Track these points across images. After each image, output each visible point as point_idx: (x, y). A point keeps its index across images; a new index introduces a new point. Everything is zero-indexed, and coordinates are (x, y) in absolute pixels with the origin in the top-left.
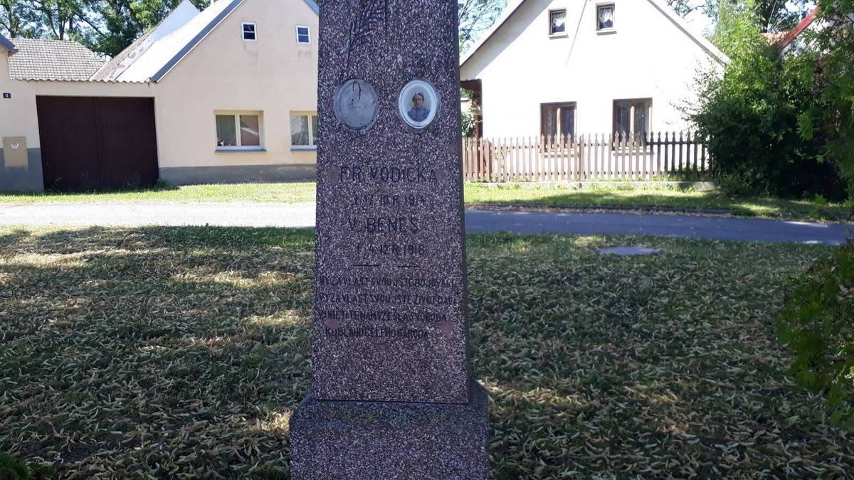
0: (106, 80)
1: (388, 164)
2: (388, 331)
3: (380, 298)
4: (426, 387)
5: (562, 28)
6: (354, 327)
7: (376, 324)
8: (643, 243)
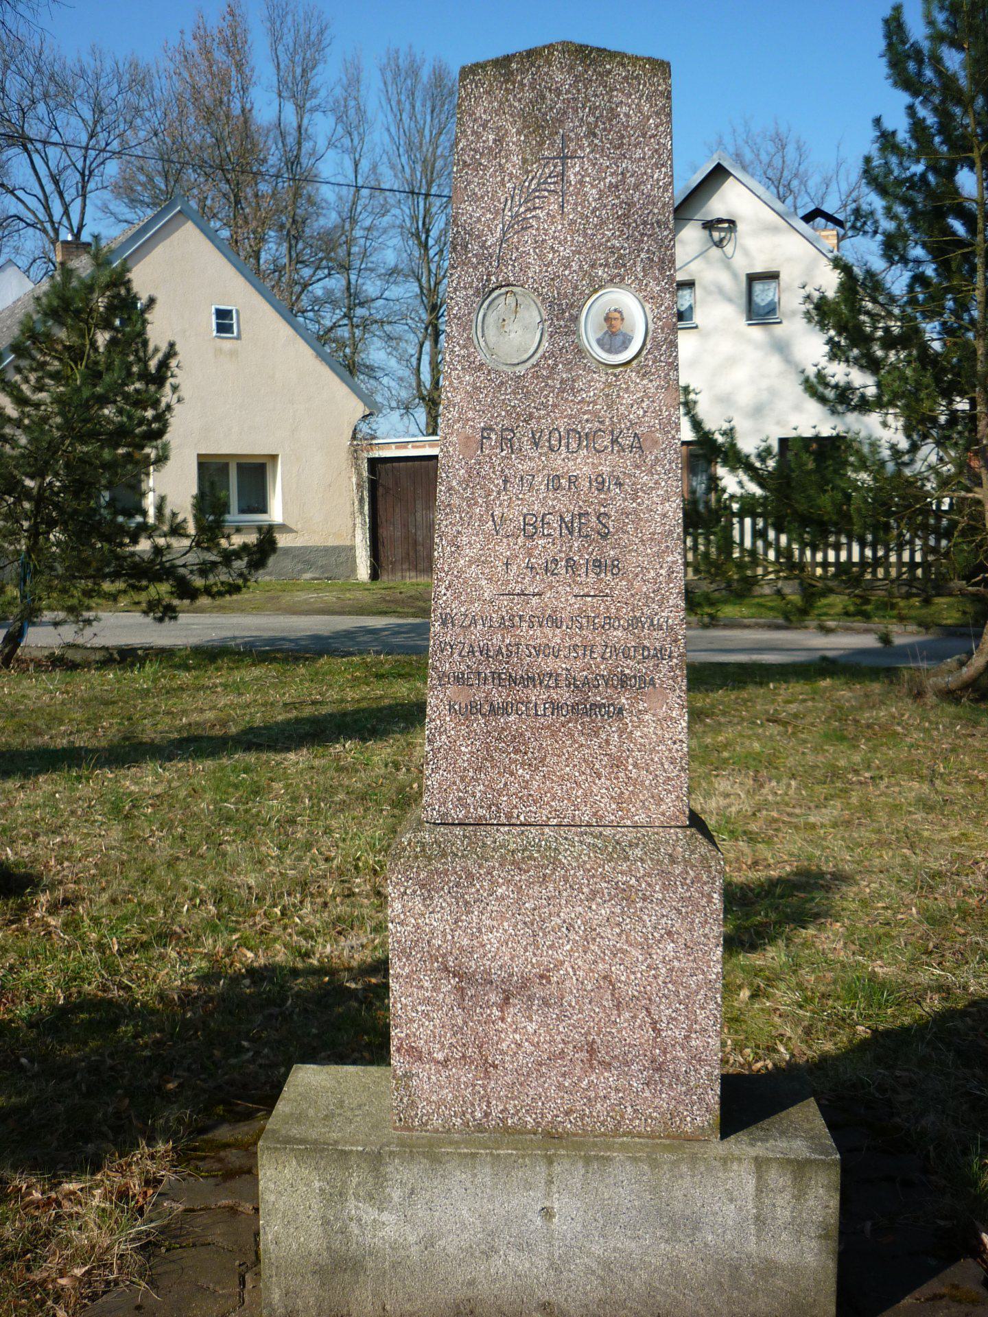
1: (562, 424)
2: (556, 707)
4: (619, 800)
6: (498, 700)
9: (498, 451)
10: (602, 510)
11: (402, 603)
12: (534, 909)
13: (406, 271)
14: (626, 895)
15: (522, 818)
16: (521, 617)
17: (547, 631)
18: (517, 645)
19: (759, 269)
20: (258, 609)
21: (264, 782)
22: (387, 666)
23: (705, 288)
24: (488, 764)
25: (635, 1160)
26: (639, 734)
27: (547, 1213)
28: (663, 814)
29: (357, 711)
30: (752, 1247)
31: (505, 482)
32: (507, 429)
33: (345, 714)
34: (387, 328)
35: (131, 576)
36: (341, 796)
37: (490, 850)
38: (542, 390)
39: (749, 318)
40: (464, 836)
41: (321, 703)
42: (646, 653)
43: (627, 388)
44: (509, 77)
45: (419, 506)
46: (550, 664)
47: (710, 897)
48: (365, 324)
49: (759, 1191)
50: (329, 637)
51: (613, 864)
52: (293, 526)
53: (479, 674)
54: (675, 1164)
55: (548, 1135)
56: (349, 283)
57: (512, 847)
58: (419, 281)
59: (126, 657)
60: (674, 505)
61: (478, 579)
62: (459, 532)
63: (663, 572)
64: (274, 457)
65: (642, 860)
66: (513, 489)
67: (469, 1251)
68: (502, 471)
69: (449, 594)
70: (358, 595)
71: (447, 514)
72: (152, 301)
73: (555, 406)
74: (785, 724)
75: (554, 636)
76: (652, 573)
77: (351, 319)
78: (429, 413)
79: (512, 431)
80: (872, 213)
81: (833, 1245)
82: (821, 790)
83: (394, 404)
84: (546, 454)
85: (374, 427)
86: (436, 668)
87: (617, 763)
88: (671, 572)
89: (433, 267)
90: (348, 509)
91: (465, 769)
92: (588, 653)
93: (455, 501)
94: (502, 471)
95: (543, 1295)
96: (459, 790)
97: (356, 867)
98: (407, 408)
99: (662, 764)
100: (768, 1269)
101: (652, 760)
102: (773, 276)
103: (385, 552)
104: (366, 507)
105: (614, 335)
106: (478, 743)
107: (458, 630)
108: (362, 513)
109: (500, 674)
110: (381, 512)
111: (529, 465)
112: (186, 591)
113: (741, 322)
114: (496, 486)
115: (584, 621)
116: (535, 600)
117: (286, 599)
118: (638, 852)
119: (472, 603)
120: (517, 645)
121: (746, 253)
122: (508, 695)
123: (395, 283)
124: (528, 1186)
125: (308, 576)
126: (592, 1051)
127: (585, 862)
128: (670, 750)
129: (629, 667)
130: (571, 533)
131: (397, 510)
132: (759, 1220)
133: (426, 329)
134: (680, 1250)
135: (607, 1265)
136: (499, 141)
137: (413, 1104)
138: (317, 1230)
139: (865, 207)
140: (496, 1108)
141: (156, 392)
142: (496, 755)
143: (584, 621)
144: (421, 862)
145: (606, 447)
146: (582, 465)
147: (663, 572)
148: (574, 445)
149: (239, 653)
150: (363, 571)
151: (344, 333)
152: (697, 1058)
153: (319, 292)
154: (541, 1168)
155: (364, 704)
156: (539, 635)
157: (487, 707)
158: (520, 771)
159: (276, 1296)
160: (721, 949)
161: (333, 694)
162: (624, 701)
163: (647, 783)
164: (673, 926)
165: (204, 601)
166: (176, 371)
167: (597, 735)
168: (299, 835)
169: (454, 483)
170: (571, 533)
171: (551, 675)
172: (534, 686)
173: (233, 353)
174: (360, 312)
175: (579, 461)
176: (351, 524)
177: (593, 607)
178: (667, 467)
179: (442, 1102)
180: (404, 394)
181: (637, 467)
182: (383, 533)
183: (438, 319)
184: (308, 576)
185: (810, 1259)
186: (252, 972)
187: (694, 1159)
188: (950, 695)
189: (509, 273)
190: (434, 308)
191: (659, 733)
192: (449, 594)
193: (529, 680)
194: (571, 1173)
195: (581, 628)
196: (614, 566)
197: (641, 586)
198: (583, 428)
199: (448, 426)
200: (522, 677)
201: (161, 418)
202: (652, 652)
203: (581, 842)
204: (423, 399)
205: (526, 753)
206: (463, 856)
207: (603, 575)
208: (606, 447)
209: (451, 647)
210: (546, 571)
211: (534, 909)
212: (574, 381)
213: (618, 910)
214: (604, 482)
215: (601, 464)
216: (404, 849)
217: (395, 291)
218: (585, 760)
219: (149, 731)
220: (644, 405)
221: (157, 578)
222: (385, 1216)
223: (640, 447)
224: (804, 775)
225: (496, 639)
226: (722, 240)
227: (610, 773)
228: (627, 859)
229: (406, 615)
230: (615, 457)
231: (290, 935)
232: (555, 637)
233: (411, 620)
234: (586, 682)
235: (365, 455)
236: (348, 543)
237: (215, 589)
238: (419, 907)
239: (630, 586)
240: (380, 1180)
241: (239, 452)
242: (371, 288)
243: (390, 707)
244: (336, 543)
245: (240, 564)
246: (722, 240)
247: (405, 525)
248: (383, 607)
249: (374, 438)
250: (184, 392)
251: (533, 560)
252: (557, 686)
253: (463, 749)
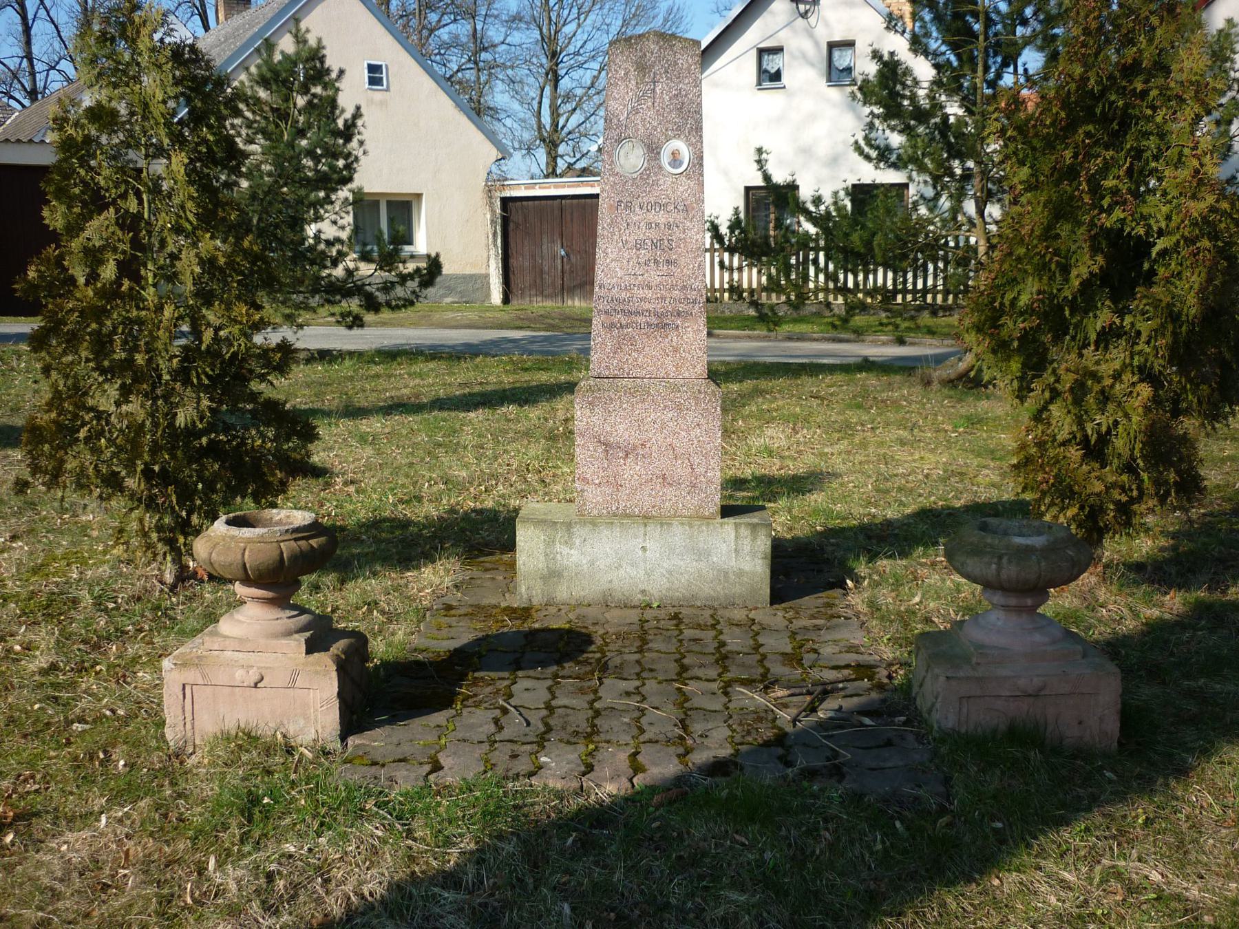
0: (36, 140)
1: (652, 200)
2: (649, 325)
3: (644, 300)
4: (677, 367)
5: (777, 76)
6: (624, 322)
7: (640, 319)
8: (1028, 846)
11: (534, 320)
13: (527, 18)
14: (679, 408)
19: (837, 38)
20: (415, 325)
21: (458, 426)
23: (791, 54)
25: (683, 524)
27: (644, 549)
30: (733, 563)
33: (504, 391)
34: (510, 72)
35: (327, 292)
36: (512, 435)
39: (829, 80)
44: (631, 46)
45: (545, 240)
46: (646, 306)
48: (492, 66)
49: (736, 537)
54: (700, 526)
55: (645, 517)
56: (475, 29)
58: (541, 30)
59: (324, 356)
64: (419, 196)
66: (631, 227)
67: (610, 567)
72: (342, 72)
74: (822, 399)
77: (476, 63)
78: (549, 153)
80: (901, 17)
81: (769, 562)
82: (836, 435)
83: (517, 145)
85: (504, 168)
87: (676, 350)
89: (554, 16)
90: (484, 241)
93: (606, 233)
95: (642, 587)
98: (529, 149)
100: (741, 573)
102: (850, 44)
104: (499, 240)
105: (675, 160)
108: (495, 245)
111: (637, 218)
112: (372, 305)
113: (822, 83)
117: (436, 317)
121: (827, 24)
123: (517, 29)
124: (636, 537)
125: (449, 300)
126: (664, 479)
129: (681, 307)
131: (526, 243)
132: (736, 551)
133: (547, 74)
134: (702, 565)
135: (670, 573)
136: (626, 74)
137: (584, 504)
138: (542, 558)
139: (896, 12)
140: (622, 504)
141: (344, 144)
144: (590, 393)
146: (661, 218)
149: (412, 353)
150: (496, 297)
151: (470, 75)
152: (710, 481)
153: (445, 37)
154: (642, 529)
155: (517, 385)
156: (642, 293)
159: (523, 589)
165: (386, 314)
166: (362, 129)
173: (383, 104)
174: (484, 56)
176: (485, 255)
179: (597, 503)
180: (527, 136)
183: (557, 65)
184: (449, 300)
185: (759, 569)
186: (474, 510)
187: (708, 524)
188: (951, 383)
189: (629, 132)
190: (554, 55)
193: (637, 313)
194: (654, 530)
201: (348, 167)
204: (544, 141)
217: (516, 37)
219: (361, 401)
221: (348, 294)
222: (573, 552)
224: (829, 427)
225: (623, 295)
226: (807, 12)
229: (539, 329)
232: (649, 294)
233: (542, 333)
235: (498, 194)
236: (483, 272)
237: (394, 303)
238: (588, 414)
240: (571, 535)
241: (389, 191)
242: (494, 33)
243: (537, 386)
244: (473, 272)
245: (413, 285)
246: (807, 12)
247: (533, 256)
248: (519, 323)
249: (506, 179)
250: (367, 146)
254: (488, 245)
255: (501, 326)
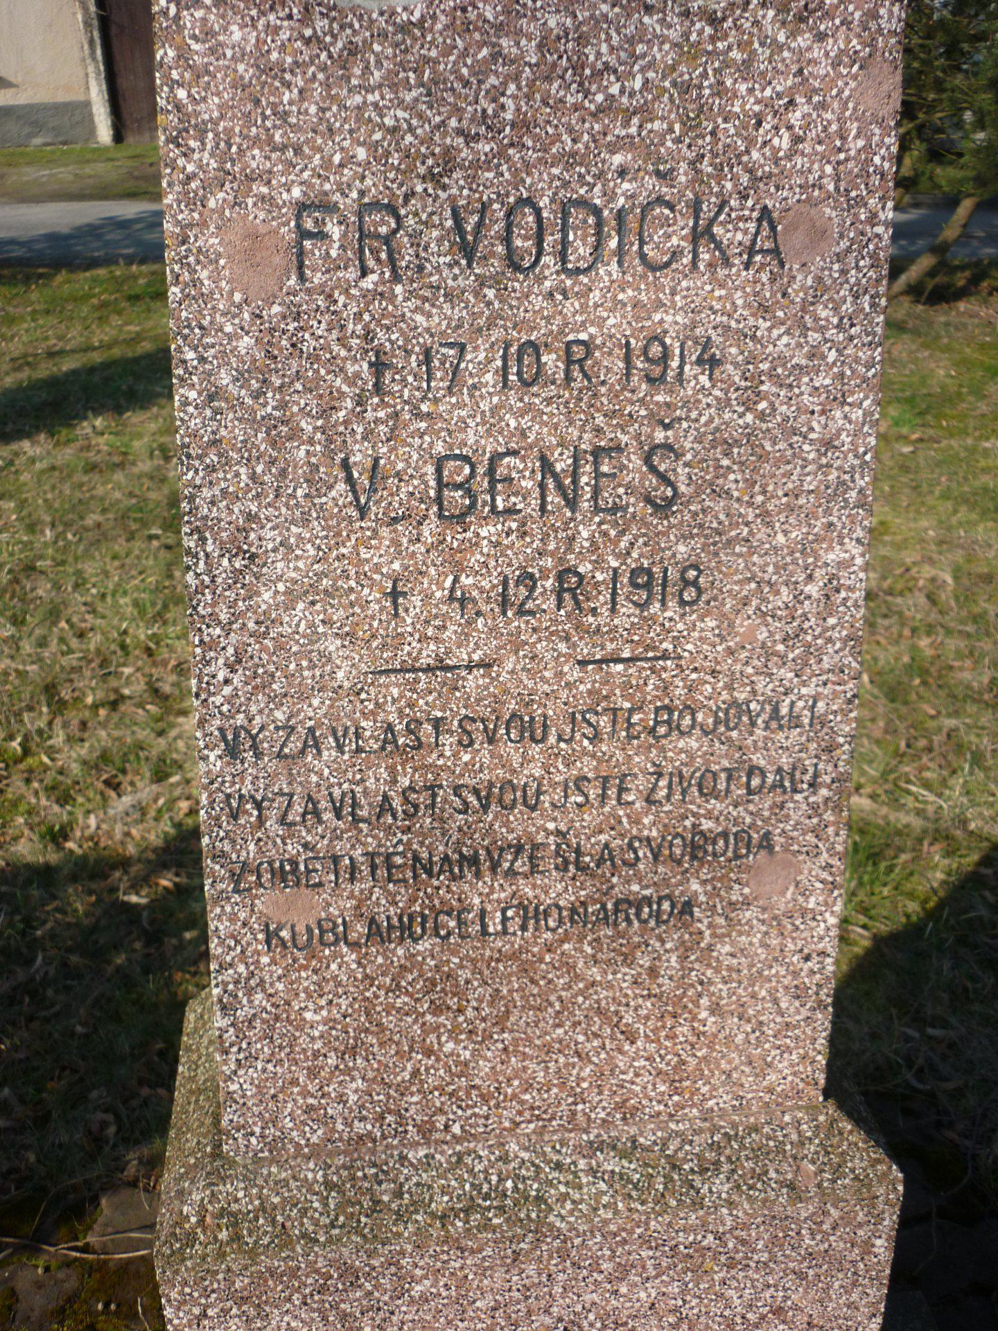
2: (532, 914)
6: (386, 912)
9: (352, 274)
10: (660, 436)
12: (494, 1309)
15: (456, 1129)
16: (437, 723)
17: (510, 750)
18: (432, 788)
22: (141, 281)
24: (372, 1039)
26: (728, 948)
28: (771, 1091)
29: (106, 365)
31: (379, 367)
32: (375, 205)
37: (389, 1219)
38: (481, 72)
40: (329, 1185)
41: (61, 353)
42: (755, 782)
43: (748, 63)
46: (517, 825)
47: (867, 1247)
50: (67, 237)
51: (667, 1218)
52: (12, 79)
53: (336, 859)
57: (441, 1203)
60: (857, 414)
61: (314, 638)
62: (250, 517)
63: (812, 589)
65: (731, 1204)
68: (368, 336)
69: (237, 680)
70: (100, 168)
71: (211, 469)
73: (523, 125)
75: (526, 760)
76: (786, 594)
79: (392, 210)
84: (496, 281)
86: (223, 854)
88: (832, 587)
91: (316, 1055)
92: (612, 793)
93: (233, 430)
94: (368, 336)
96: (305, 1093)
97: (123, 647)
99: (776, 1001)
101: (754, 996)
103: (127, 108)
104: (99, 52)
106: (344, 1003)
107: (271, 765)
108: (94, 59)
109: (388, 857)
110: (118, 57)
114: (351, 382)
115: (604, 721)
116: (473, 681)
118: (721, 1186)
119: (304, 697)
120: (432, 788)
122: (412, 900)
125: (38, 141)
127: (606, 1222)
128: (796, 974)
130: (572, 504)
142: (389, 1021)
143: (604, 721)
145: (676, 254)
147: (812, 589)
148: (581, 250)
150: (104, 132)
157: (360, 929)
158: (449, 1047)
160: (879, 1320)
161: (75, 336)
162: (695, 886)
163: (740, 1038)
164: (786, 1298)
167: (629, 960)
168: (40, 592)
169: (224, 378)
170: (572, 504)
171: (519, 849)
172: (478, 875)
175: (595, 296)
176: (82, 75)
177: (627, 685)
178: (847, 307)
181: (764, 310)
182: (123, 83)
191: (775, 942)
192: (237, 680)
195: (596, 738)
196: (686, 583)
197: (752, 630)
198: (610, 196)
199: (190, 201)
200: (446, 858)
202: (770, 778)
203: (592, 1171)
205: (460, 1011)
206: (330, 1241)
207: (655, 607)
208: (676, 254)
209: (258, 805)
210: (504, 603)
211: (494, 1309)
212: (582, 40)
213: (675, 1289)
214: (666, 356)
215: (659, 305)
216: (191, 1239)
218: (599, 1012)
220: (795, 118)
223: (776, 252)
227: (655, 1030)
228: (698, 1204)
230: (698, 285)
231: (36, 793)
234: (606, 856)
236: (82, 98)
239: (727, 627)
251: (466, 581)
252: (534, 869)
253: (308, 1015)
254: (83, 60)
255: (104, 193)
